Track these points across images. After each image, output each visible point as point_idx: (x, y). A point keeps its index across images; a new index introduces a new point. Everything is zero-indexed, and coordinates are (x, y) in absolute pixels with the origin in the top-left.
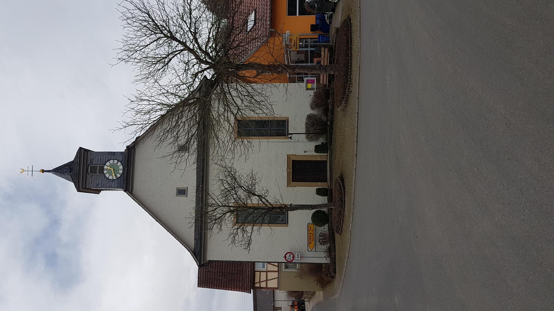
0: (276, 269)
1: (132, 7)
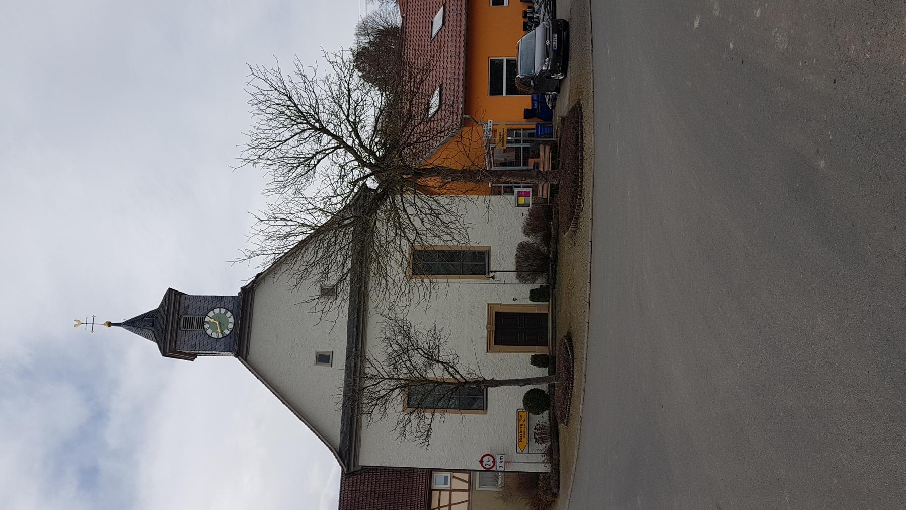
0: (465, 486)
1: (266, 86)
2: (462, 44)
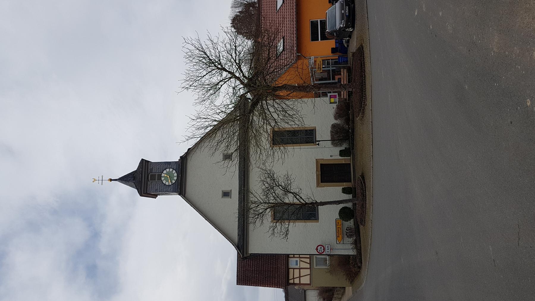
0: (308, 266)
2: (295, 13)
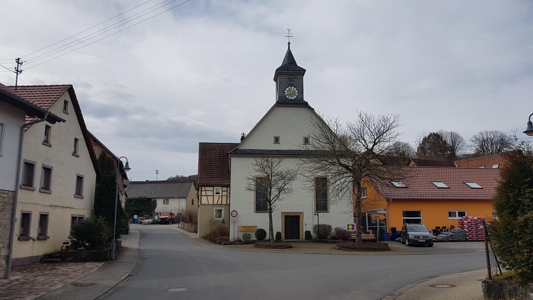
0: (215, 203)
